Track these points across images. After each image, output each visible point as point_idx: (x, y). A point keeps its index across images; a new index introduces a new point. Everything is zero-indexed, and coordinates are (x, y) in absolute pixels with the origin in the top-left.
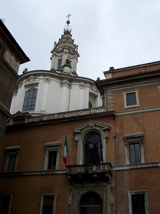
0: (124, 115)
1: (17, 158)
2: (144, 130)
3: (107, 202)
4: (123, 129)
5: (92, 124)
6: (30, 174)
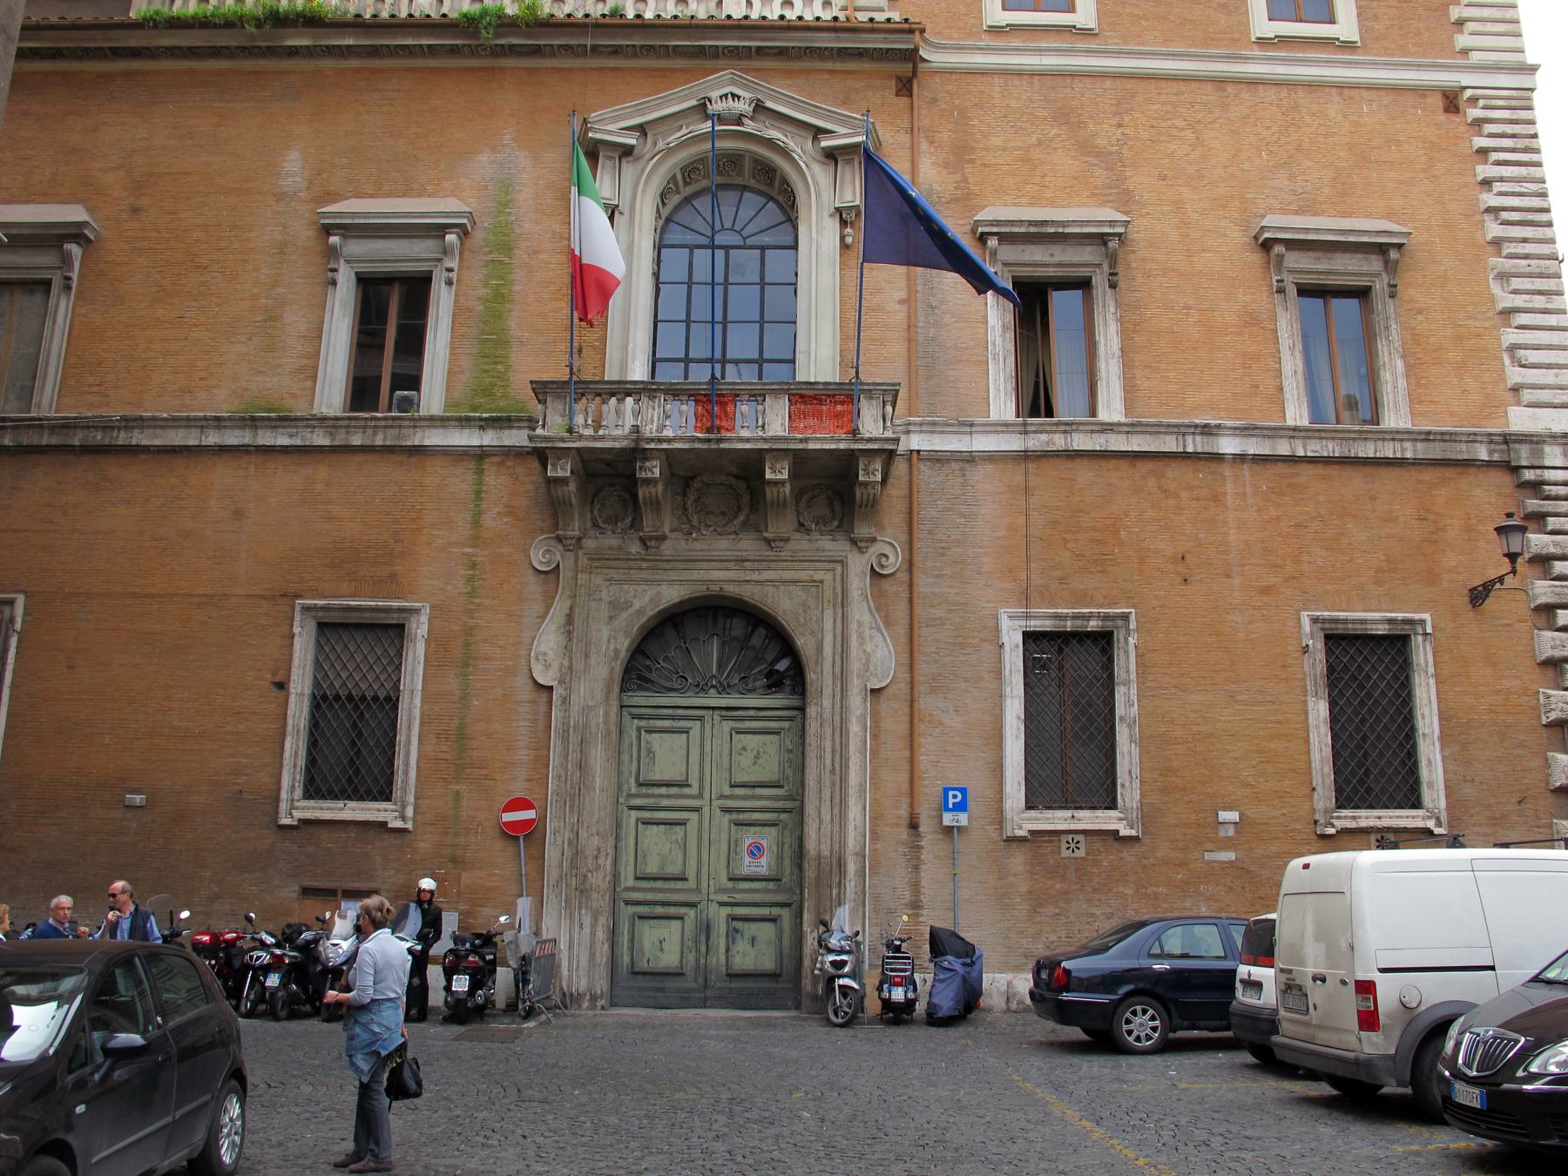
0: (984, 72)
1: (63, 308)
2: (1125, 199)
3: (842, 678)
4: (969, 169)
5: (733, 95)
6: (176, 438)
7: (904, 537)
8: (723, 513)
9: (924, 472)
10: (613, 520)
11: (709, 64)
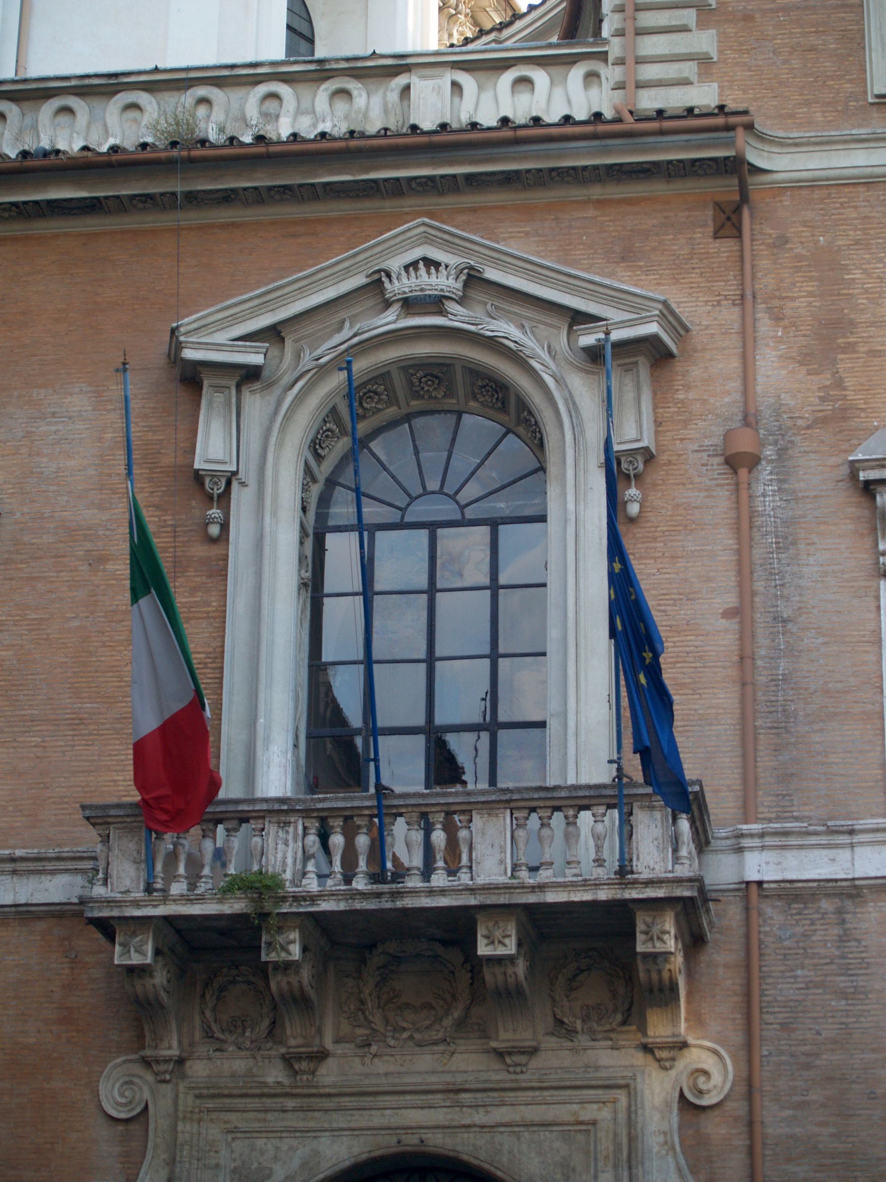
4: (844, 363)
5: (431, 264)
7: (738, 1038)
8: (428, 1006)
9: (773, 915)
10: (237, 1025)
11: (388, 205)
